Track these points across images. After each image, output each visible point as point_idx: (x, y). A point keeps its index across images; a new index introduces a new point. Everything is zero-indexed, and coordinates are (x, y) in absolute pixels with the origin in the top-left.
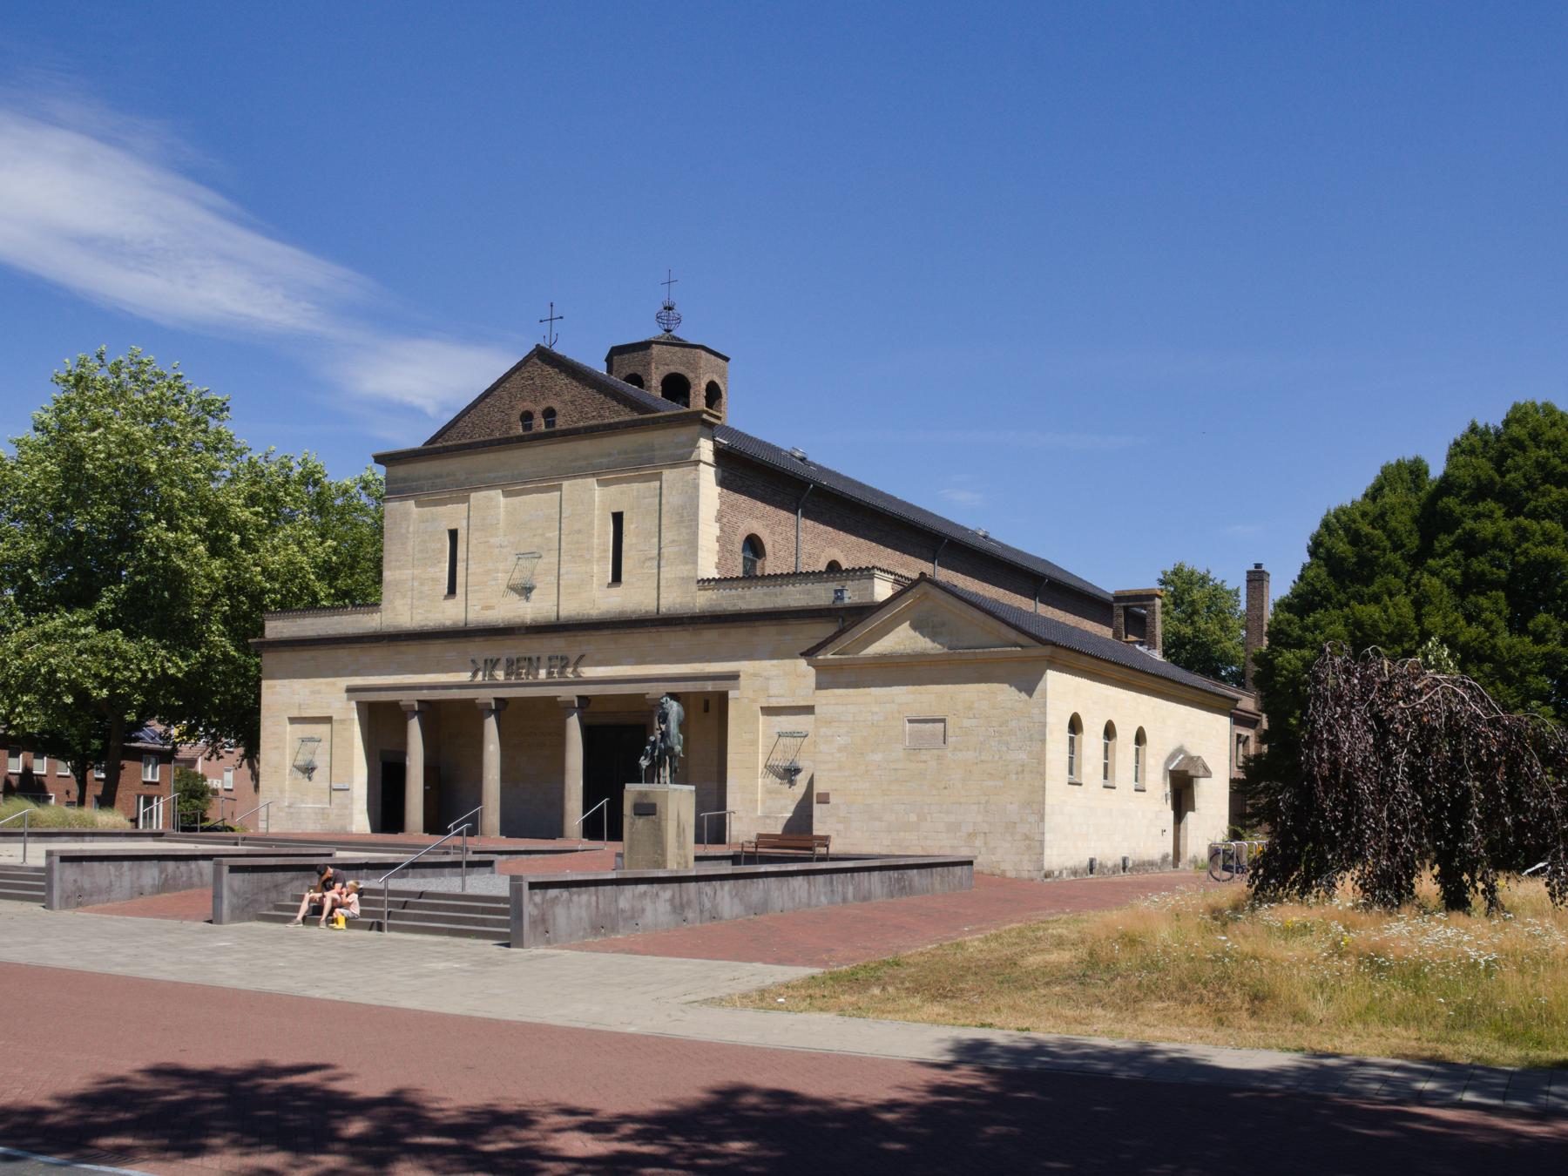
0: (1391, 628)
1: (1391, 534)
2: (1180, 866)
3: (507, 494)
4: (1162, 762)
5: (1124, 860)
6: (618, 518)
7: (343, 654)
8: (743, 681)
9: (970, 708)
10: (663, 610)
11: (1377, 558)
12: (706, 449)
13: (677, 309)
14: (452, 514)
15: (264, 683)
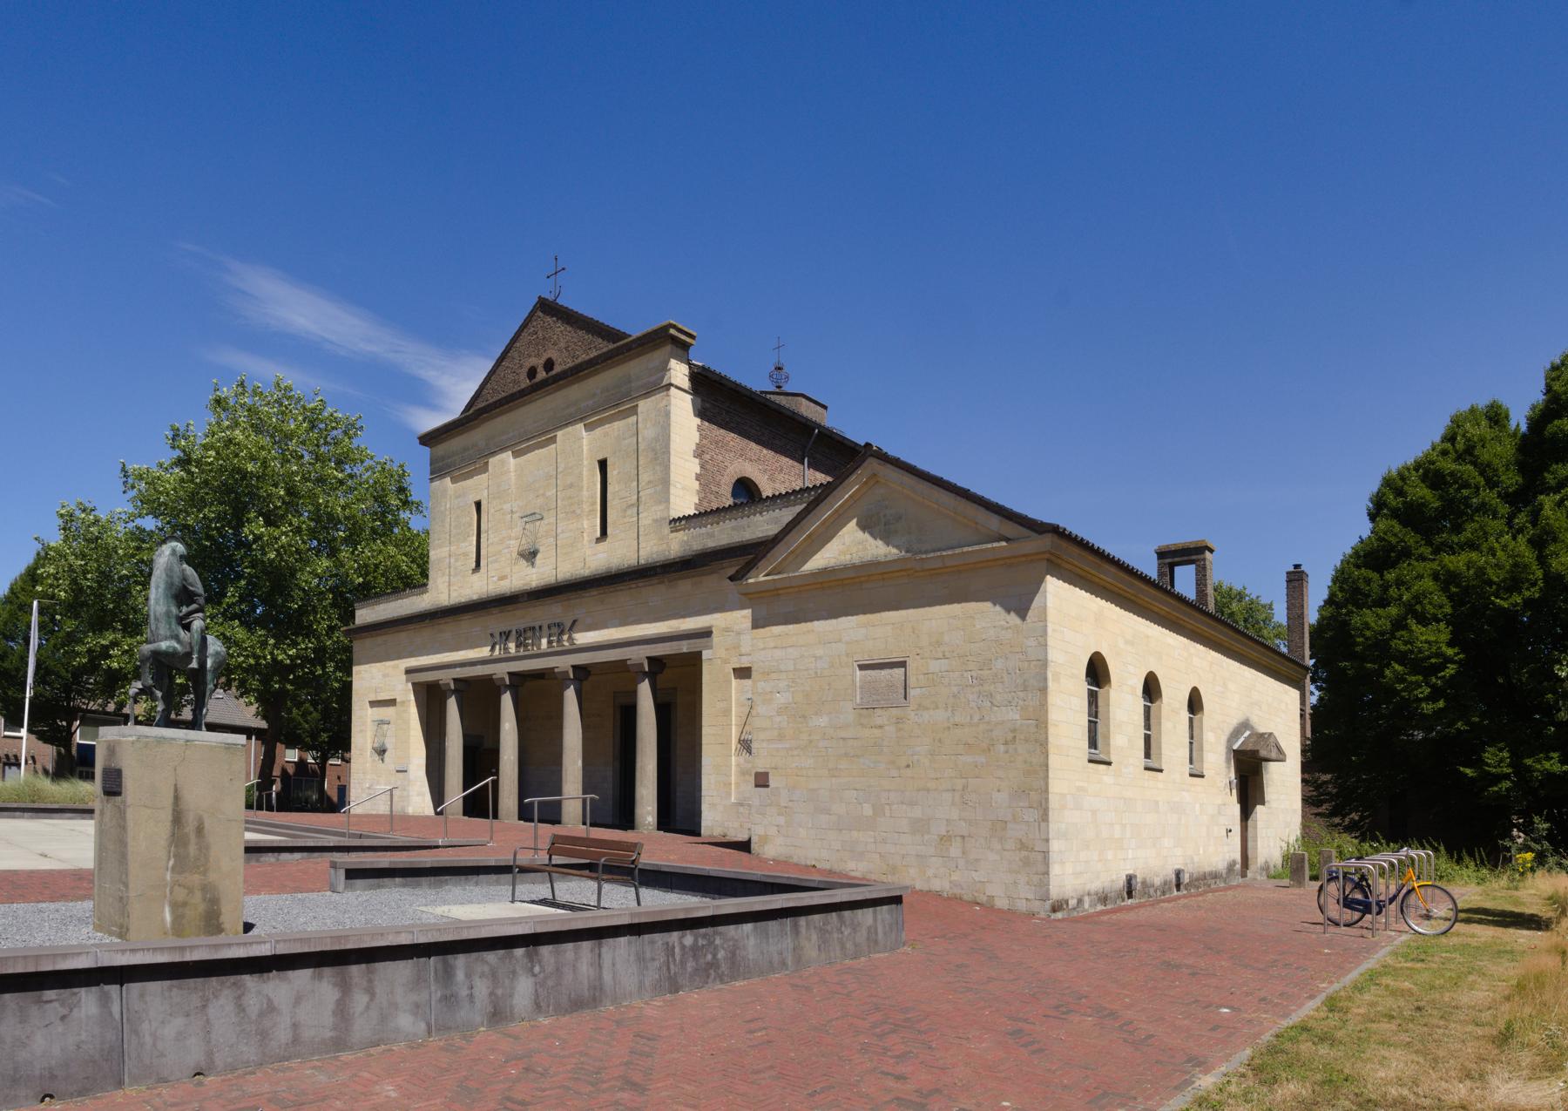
0: (1503, 574)
1: (1484, 468)
2: (1249, 874)
3: (516, 454)
4: (1224, 739)
5: (1178, 874)
6: (603, 465)
7: (403, 637)
8: (716, 638)
9: (939, 643)
10: (642, 562)
11: (1467, 498)
12: (679, 373)
13: (786, 369)
14: (476, 487)
15: (355, 669)
